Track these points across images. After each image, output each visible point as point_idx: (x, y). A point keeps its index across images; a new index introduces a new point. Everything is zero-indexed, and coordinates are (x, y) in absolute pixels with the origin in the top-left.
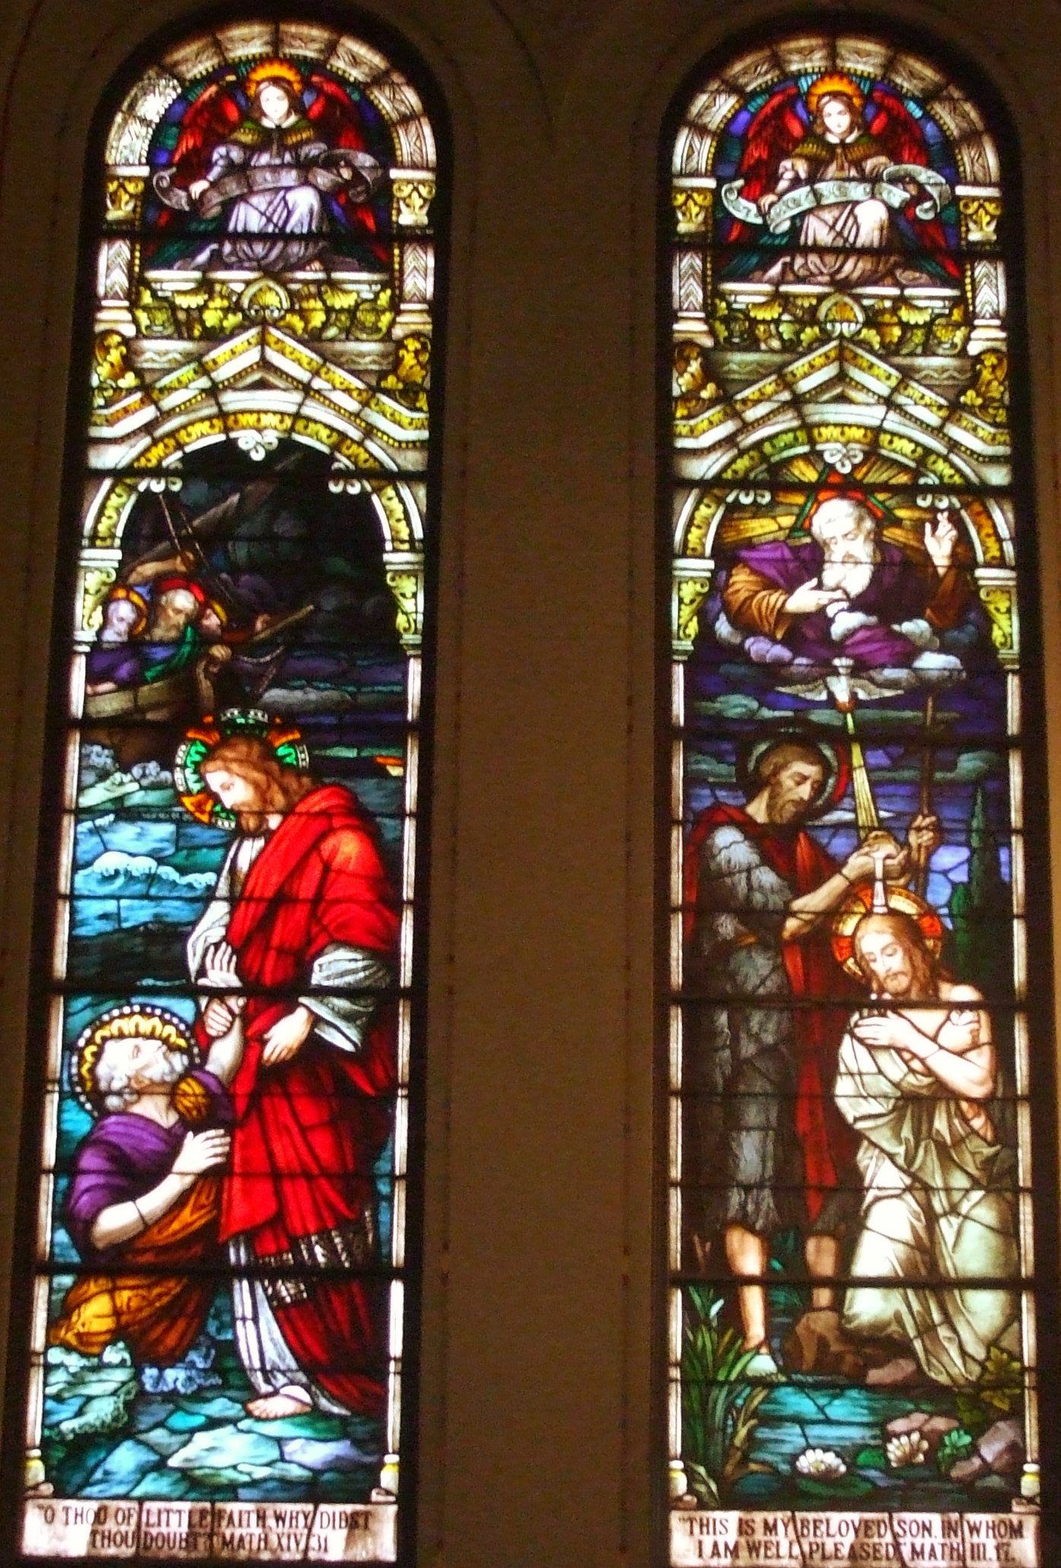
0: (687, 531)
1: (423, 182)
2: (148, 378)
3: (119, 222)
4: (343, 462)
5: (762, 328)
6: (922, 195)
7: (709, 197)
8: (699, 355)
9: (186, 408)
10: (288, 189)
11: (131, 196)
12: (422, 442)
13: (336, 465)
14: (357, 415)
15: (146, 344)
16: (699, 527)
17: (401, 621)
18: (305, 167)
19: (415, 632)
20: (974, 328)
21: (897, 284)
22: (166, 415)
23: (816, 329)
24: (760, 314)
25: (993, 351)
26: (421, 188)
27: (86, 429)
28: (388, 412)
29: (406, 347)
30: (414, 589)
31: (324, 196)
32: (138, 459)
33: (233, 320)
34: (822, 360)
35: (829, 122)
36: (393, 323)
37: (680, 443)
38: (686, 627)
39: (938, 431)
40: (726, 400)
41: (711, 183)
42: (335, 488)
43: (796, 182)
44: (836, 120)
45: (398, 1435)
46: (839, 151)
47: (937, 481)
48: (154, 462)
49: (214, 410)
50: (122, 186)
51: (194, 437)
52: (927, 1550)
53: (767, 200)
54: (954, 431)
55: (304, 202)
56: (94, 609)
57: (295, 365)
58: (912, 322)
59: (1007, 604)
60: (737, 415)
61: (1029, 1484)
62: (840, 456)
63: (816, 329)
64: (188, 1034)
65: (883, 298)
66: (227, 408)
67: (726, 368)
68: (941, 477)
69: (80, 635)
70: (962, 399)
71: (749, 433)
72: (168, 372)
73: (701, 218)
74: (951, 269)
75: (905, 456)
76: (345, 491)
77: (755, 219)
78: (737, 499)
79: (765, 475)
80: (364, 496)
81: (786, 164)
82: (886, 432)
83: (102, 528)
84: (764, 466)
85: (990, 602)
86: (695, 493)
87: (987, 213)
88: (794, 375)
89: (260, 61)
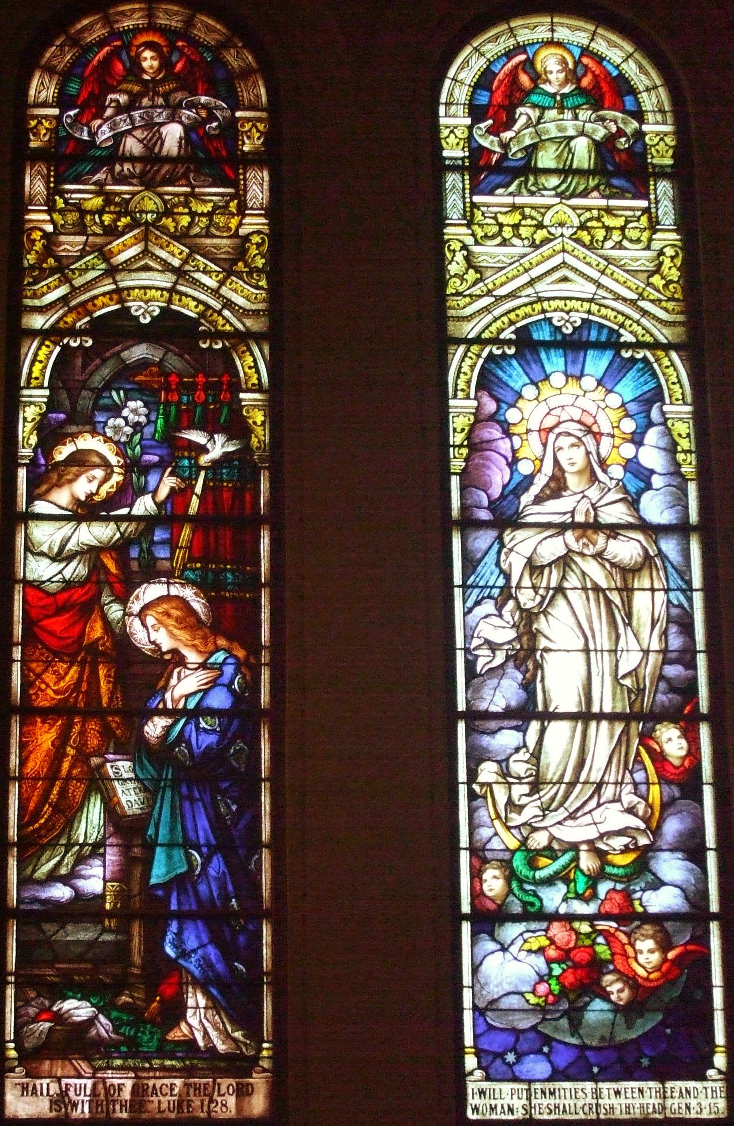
0: (32, 364)
1: (259, 120)
5: (88, 217)
7: (54, 121)
9: (90, 285)
11: (47, 129)
14: (73, 289)
15: (63, 238)
19: (264, 451)
20: (244, 216)
21: (189, 185)
23: (129, 218)
25: (258, 232)
26: (258, 124)
29: (250, 241)
30: (688, 431)
31: (187, 128)
34: (133, 241)
35: (146, 64)
36: (240, 224)
37: (28, 302)
39: (215, 293)
41: (55, 111)
43: (120, 109)
44: (149, 61)
45: (270, 1029)
46: (151, 85)
50: (40, 122)
53: (507, 135)
55: (173, 133)
56: (32, 433)
58: (611, 226)
59: (263, 418)
60: (68, 281)
62: (142, 311)
63: (129, 218)
73: (46, 138)
76: (81, 345)
78: (68, 342)
79: (513, 337)
81: (520, 110)
85: (249, 417)
86: (462, 349)
88: (112, 252)
89: (137, 31)
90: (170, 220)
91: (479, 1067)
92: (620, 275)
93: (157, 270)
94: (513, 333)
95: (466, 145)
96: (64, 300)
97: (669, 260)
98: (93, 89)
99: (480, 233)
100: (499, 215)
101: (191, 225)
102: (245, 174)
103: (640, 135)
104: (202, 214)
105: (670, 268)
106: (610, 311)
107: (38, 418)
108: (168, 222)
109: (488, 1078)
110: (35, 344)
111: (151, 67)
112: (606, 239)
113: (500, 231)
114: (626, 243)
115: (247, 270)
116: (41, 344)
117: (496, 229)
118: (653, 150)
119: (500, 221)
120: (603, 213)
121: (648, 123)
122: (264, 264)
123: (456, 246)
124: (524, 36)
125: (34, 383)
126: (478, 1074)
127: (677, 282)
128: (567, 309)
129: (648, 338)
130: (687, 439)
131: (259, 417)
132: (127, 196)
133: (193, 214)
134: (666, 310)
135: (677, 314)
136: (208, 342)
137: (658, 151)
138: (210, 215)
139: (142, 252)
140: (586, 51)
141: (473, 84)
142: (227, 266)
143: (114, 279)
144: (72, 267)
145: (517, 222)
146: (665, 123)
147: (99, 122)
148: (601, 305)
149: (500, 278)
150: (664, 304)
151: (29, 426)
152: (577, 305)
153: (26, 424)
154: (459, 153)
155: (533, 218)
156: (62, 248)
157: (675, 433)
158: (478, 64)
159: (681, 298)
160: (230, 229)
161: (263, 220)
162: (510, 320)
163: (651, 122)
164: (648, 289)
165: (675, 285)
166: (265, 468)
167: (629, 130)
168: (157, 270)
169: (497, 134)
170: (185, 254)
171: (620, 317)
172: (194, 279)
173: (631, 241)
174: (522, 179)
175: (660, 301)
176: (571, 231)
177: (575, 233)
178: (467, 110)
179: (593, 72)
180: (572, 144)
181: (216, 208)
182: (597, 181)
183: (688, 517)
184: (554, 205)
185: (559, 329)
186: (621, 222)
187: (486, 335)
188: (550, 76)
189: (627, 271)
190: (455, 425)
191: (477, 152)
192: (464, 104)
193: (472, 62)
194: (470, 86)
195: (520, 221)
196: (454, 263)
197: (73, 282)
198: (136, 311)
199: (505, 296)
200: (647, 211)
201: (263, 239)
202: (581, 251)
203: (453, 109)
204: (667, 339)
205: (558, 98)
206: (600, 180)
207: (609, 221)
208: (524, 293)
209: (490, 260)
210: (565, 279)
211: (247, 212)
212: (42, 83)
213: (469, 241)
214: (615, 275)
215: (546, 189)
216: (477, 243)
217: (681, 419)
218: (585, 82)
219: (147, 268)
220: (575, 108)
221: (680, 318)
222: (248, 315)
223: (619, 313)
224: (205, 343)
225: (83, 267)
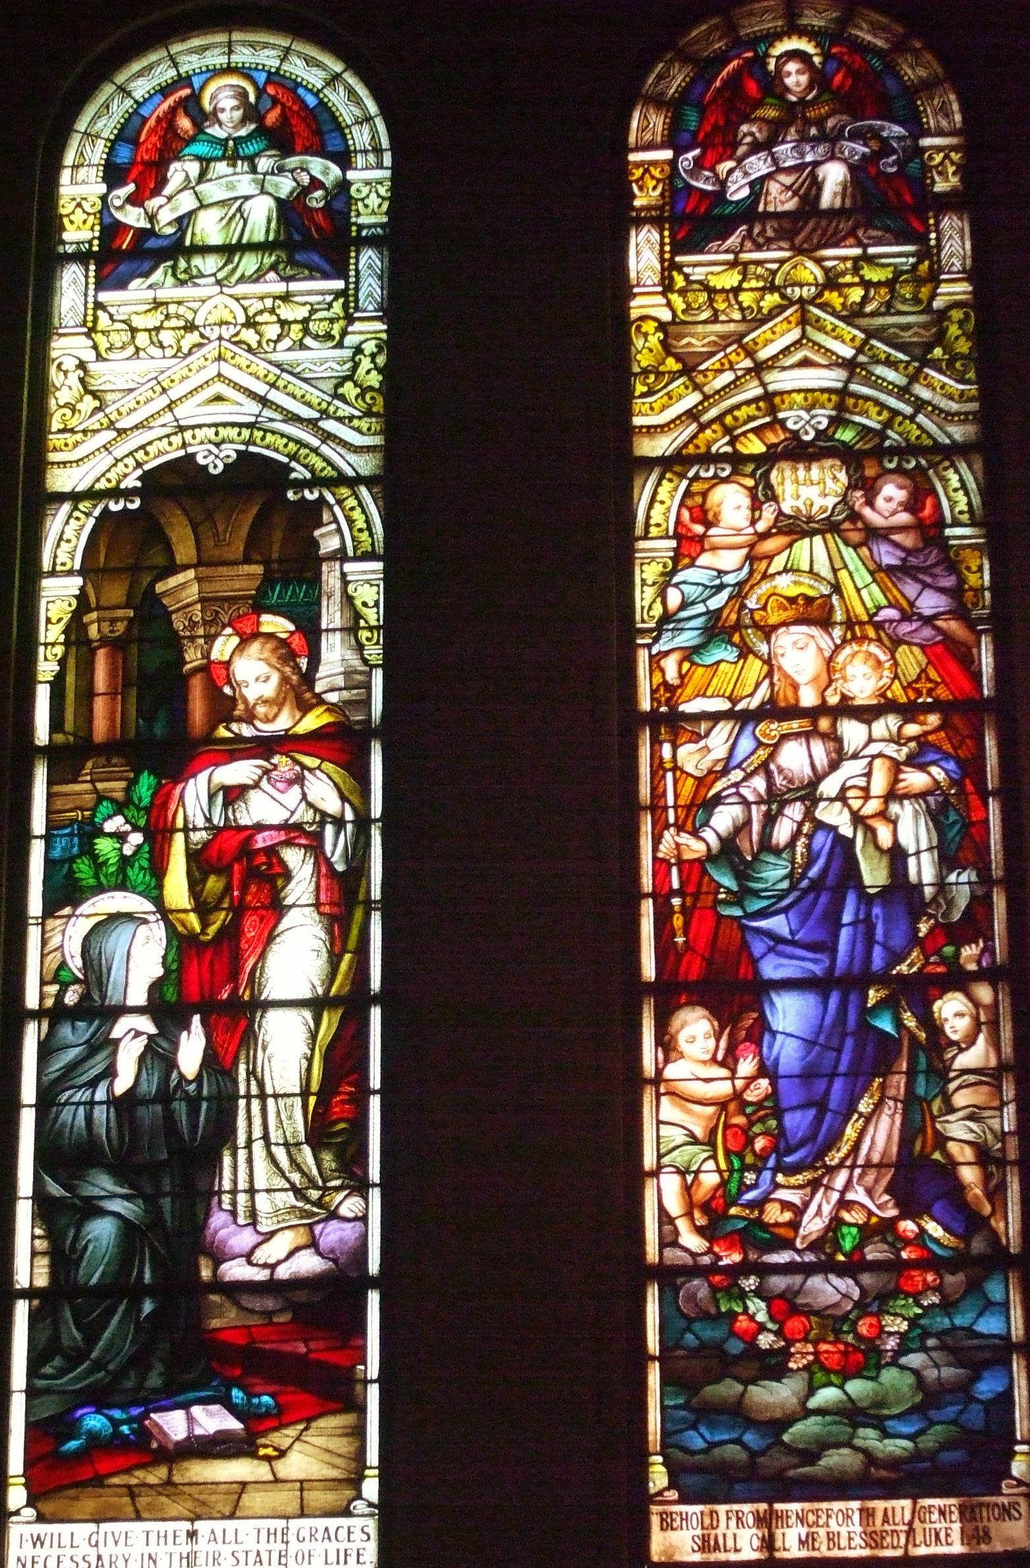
1: (953, 148)
3: (648, 208)
6: (885, 148)
7: (667, 168)
8: (657, 329)
10: (247, 198)
12: (974, 413)
13: (293, 475)
14: (706, 397)
18: (831, 140)
19: (377, 643)
21: (859, 244)
28: (937, 385)
29: (949, 319)
33: (772, 299)
35: (789, 81)
37: (638, 421)
38: (650, 608)
39: (903, 392)
43: (755, 148)
47: (308, 475)
50: (646, 171)
51: (152, 455)
53: (153, 203)
55: (834, 175)
57: (252, 379)
61: (371, 1488)
62: (803, 422)
63: (776, 296)
65: (844, 259)
68: (313, 471)
74: (916, 224)
77: (144, 224)
78: (106, 507)
79: (139, 484)
86: (66, 507)
87: (653, 177)
91: (29, 1504)
92: (299, 387)
95: (97, 221)
96: (692, 415)
97: (369, 359)
98: (717, 120)
99: (103, 342)
100: (134, 317)
101: (865, 300)
102: (937, 224)
103: (344, 185)
104: (879, 284)
105: (368, 372)
108: (833, 298)
109: (41, 1518)
111: (798, 84)
112: (280, 338)
113: (711, 301)
114: (308, 341)
116: (661, 478)
117: (126, 337)
118: (360, 204)
119: (134, 325)
120: (278, 302)
121: (356, 169)
123: (70, 364)
124: (190, 63)
125: (654, 531)
126: (30, 1513)
127: (378, 391)
129: (329, 472)
130: (375, 610)
132: (775, 266)
134: (358, 430)
135: (373, 435)
136: (896, 459)
137: (366, 206)
138: (890, 284)
140: (275, 77)
141: (112, 137)
142: (918, 351)
143: (760, 379)
144: (702, 367)
145: (736, 284)
146: (380, 166)
147: (730, 164)
148: (265, 431)
149: (129, 402)
150: (356, 423)
152: (232, 432)
154: (86, 235)
155: (178, 317)
156: (685, 341)
157: (358, 603)
158: (120, 109)
159: (382, 411)
162: (136, 461)
163: (359, 166)
164: (336, 402)
165: (375, 394)
167: (329, 181)
169: (141, 205)
171: (291, 445)
173: (316, 337)
174: (169, 263)
175: (351, 418)
176: (233, 331)
178: (101, 174)
179: (283, 105)
180: (247, 206)
181: (898, 273)
182: (273, 258)
183: (90, 729)
184: (210, 298)
185: (795, 434)
186: (303, 312)
187: (102, 485)
188: (222, 116)
189: (305, 380)
191: (111, 229)
192: (97, 165)
193: (114, 107)
194: (348, 126)
195: (162, 322)
196: (65, 389)
198: (795, 423)
199: (131, 429)
200: (342, 293)
202: (244, 358)
203: (82, 173)
204: (354, 470)
205: (231, 143)
206: (278, 256)
207: (286, 312)
208: (161, 421)
210: (219, 398)
211: (943, 277)
212: (82, 153)
213: (89, 355)
214: (290, 386)
215: (203, 276)
216: (99, 357)
217: (368, 582)
218: (272, 118)
219: (806, 363)
220: (251, 160)
221: (377, 440)
222: (952, 421)
223: (290, 439)
224: (890, 461)
225: (717, 366)
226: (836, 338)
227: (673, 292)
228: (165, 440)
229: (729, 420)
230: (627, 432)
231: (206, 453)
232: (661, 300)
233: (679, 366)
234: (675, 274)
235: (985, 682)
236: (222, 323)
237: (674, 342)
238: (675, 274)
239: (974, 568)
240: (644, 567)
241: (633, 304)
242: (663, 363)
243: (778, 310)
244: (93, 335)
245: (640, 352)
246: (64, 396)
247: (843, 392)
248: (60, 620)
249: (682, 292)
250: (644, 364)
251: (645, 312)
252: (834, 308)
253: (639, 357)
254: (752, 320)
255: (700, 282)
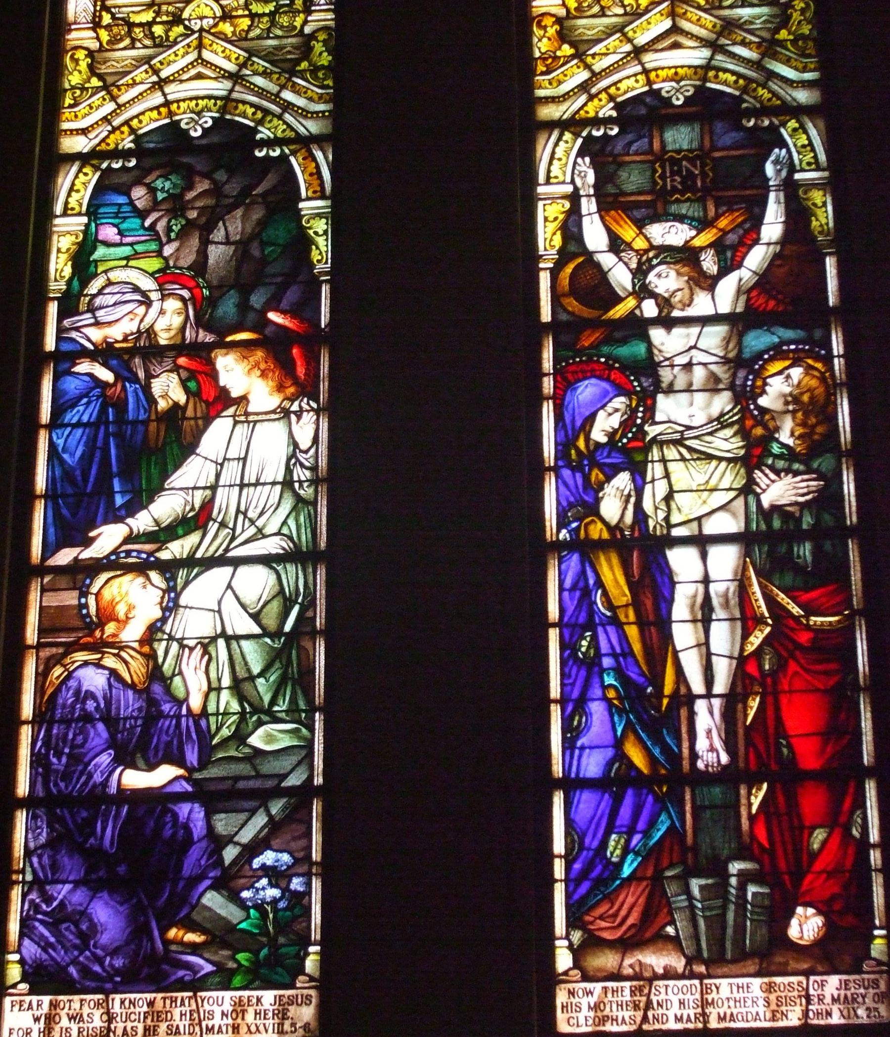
2: (110, 80)
4: (264, 133)
8: (86, 56)
13: (259, 136)
16: (560, 159)
17: (315, 256)
19: (326, 263)
22: (596, 76)
24: (136, 19)
27: (533, 93)
30: (325, 227)
32: (99, 144)
36: (306, 22)
38: (551, 240)
39: (275, 98)
40: (109, 88)
42: (258, 154)
48: (112, 146)
49: (639, 68)
52: (685, 1017)
54: (287, 95)
64: (654, 565)
66: (648, 66)
67: (577, 33)
69: (53, 285)
70: (777, 36)
71: (599, 81)
72: (599, 41)
75: (728, 86)
76: (605, 134)
78: (590, 133)
79: (132, 145)
80: (283, 158)
82: (172, 102)
83: (73, 203)
84: (612, 105)
85: (310, 228)
90: (228, 24)
93: (210, 78)
94: (131, 142)
96: (584, 87)
106: (627, 80)
107: (561, 217)
108: (226, 28)
109: (31, 992)
110: (75, 169)
113: (129, 33)
115: (791, 37)
122: (810, 30)
126: (24, 987)
128: (678, 78)
130: (325, 237)
131: (321, 225)
133: (252, 16)
139: (196, 60)
144: (591, 52)
145: (150, 19)
151: (552, 227)
153: (60, 255)
160: (295, 28)
161: (331, 16)
166: (830, 254)
168: (210, 78)
170: (718, 26)
172: (251, 83)
177: (216, 25)
190: (547, 214)
197: (594, 67)
198: (187, 124)
201: (329, 34)
209: (119, 66)
219: (199, 76)
224: (260, 151)
226: (169, 64)
227: (101, 27)
228: (633, 79)
229: (135, 123)
230: (531, 102)
231: (670, 89)
232: (91, 34)
233: (100, 84)
234: (104, 13)
235: (830, 294)
236: (201, 18)
237: (99, 66)
238: (104, 13)
239: (820, 204)
240: (547, 207)
241: (69, 37)
242: (89, 81)
243: (223, 36)
244: (98, 30)
245: (71, 73)
246: (75, 79)
247: (227, 99)
248: (556, 219)
249: (108, 27)
250: (73, 83)
251: (543, 10)
252: (225, 35)
253: (70, 77)
254: (633, 14)
255: (123, 19)
